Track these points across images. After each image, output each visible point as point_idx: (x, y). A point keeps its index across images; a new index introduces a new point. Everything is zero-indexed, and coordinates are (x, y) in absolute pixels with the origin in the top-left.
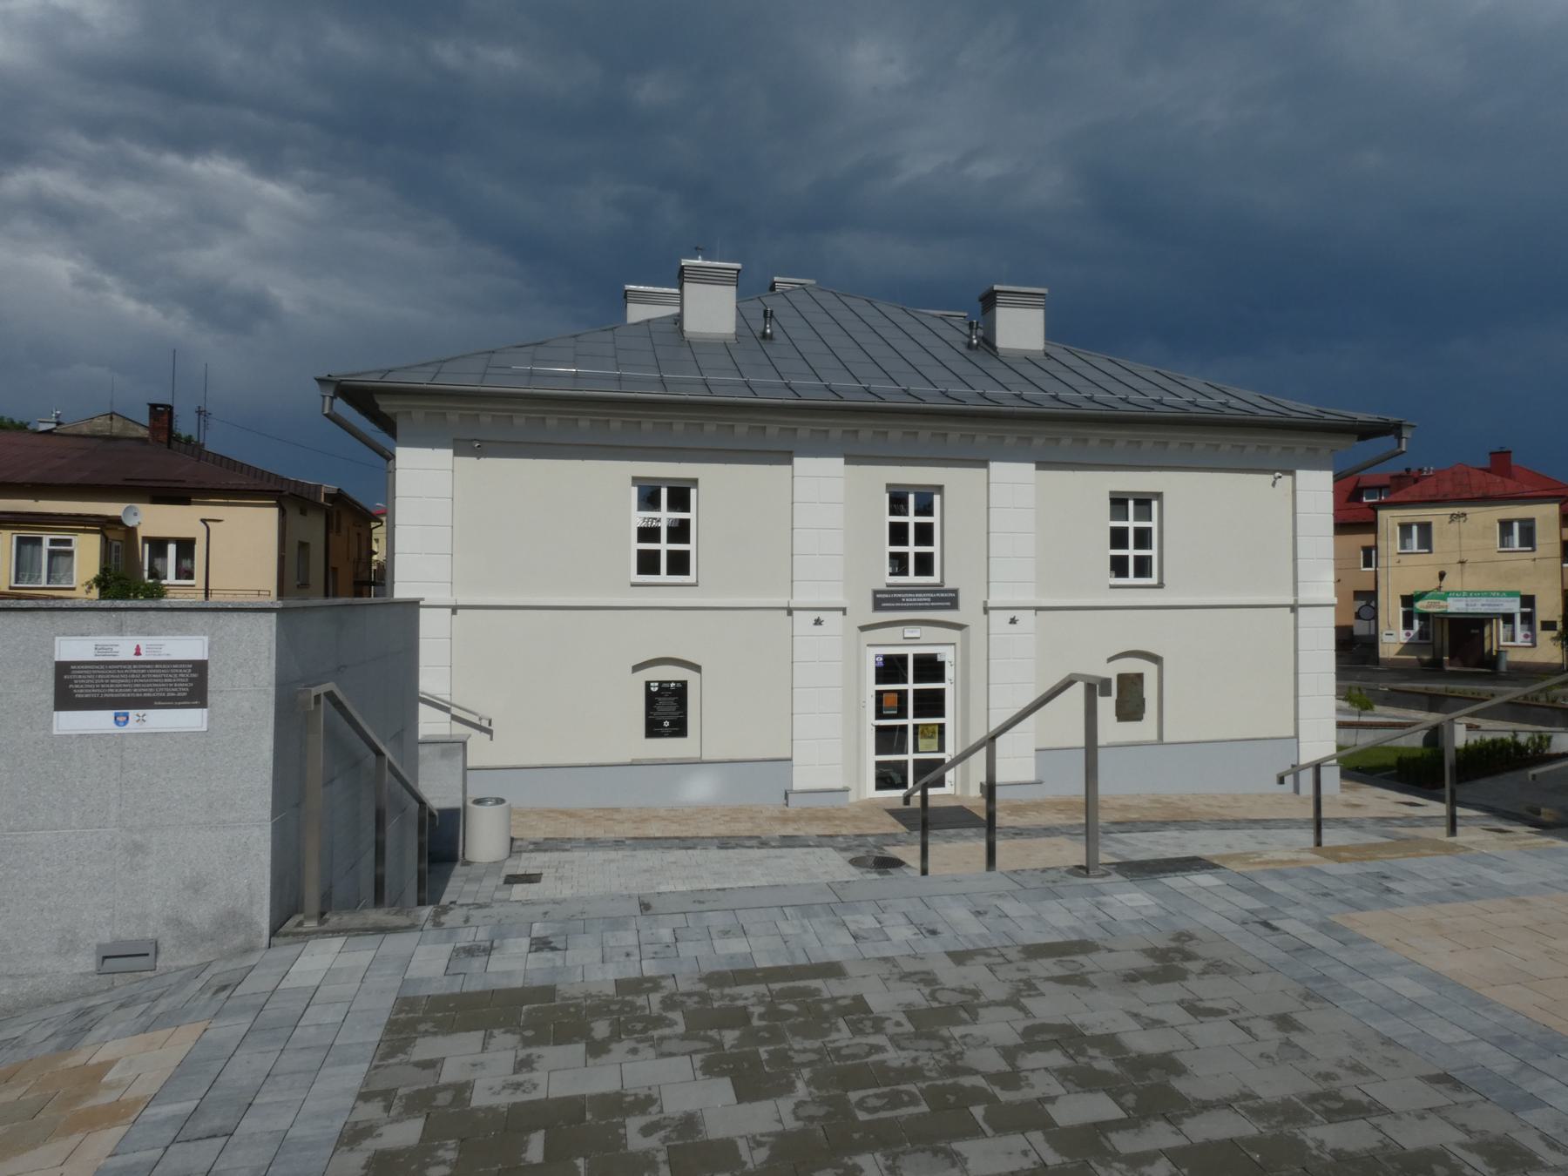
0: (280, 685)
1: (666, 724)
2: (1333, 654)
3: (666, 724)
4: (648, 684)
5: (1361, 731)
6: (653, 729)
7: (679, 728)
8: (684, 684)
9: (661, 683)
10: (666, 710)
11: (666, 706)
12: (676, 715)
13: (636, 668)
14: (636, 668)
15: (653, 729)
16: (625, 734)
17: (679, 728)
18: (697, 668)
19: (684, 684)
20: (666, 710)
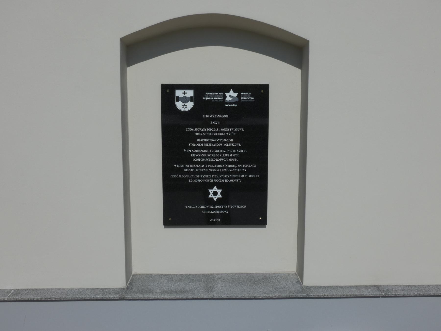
0: (52, 289)
1: (215, 193)
2: (227, 273)
3: (215, 193)
4: (168, 92)
5: (19, 299)
6: (183, 205)
7: (247, 205)
8: (261, 93)
9: (200, 90)
10: (216, 161)
11: (213, 148)
12: (238, 173)
13: (138, 48)
14: (138, 48)
15: (183, 205)
16: (91, 200)
17: (247, 205)
18: (293, 50)
19: (261, 93)
20: (216, 161)
